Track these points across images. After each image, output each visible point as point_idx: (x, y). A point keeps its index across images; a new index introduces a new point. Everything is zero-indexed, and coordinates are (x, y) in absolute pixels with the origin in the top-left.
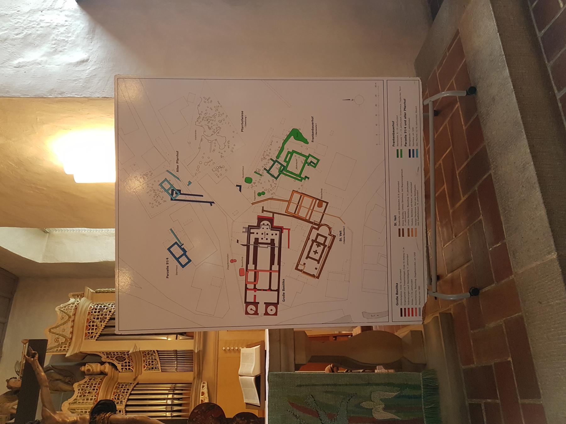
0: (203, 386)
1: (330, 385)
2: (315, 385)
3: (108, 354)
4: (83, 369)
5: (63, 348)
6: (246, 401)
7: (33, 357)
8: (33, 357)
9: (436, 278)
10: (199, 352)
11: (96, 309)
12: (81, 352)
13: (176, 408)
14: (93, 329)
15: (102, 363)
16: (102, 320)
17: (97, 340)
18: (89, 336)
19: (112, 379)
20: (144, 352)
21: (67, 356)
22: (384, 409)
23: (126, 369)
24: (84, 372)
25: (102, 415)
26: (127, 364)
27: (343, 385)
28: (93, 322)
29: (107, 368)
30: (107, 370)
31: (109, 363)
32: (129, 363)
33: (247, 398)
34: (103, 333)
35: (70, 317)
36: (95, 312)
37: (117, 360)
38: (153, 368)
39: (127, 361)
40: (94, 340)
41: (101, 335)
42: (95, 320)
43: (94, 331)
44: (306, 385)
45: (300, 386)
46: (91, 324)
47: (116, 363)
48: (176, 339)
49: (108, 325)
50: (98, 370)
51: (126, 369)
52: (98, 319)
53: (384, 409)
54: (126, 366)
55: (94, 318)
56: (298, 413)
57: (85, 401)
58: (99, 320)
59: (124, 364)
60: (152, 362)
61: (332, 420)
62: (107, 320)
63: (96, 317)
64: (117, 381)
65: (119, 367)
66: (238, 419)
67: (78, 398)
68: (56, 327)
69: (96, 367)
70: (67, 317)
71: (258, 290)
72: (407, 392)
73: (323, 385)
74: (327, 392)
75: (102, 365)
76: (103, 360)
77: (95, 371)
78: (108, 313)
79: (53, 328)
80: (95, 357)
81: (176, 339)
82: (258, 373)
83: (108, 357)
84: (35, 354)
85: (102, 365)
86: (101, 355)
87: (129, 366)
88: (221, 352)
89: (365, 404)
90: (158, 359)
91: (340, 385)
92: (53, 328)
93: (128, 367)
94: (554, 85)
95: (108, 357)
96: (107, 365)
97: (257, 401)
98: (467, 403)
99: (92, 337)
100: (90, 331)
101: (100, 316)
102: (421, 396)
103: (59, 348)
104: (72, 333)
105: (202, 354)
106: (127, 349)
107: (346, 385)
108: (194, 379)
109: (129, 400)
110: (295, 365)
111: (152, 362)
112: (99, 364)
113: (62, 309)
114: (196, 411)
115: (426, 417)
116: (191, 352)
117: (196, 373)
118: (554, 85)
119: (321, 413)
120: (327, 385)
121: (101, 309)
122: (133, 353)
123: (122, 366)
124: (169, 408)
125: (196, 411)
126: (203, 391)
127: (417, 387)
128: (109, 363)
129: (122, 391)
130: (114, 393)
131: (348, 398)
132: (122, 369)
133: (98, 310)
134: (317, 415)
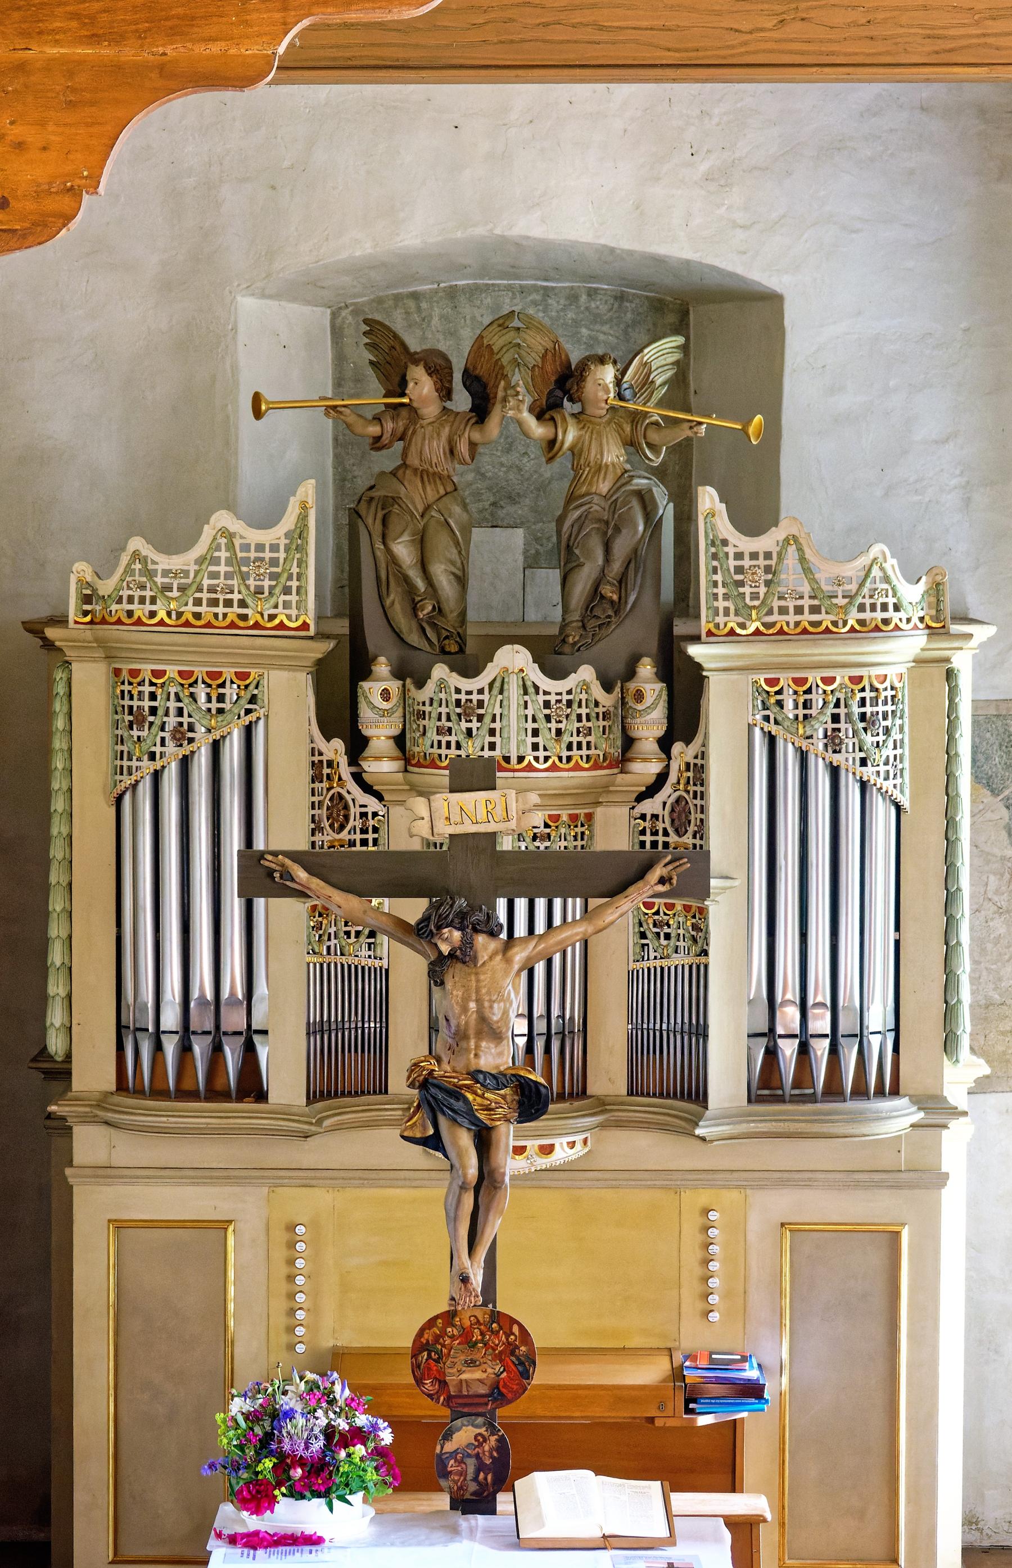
0: (572, 1145)
3: (698, 772)
5: (721, 604)
15: (665, 744)
21: (694, 650)
23: (643, 832)
29: (647, 769)
30: (636, 767)
37: (678, 800)
38: (643, 935)
47: (666, 792)
51: (643, 832)
54: (655, 833)
55: (837, 705)
57: (530, 725)
59: (660, 826)
60: (668, 936)
63: (842, 711)
65: (649, 806)
66: (493, 1438)
67: (541, 698)
68: (802, 559)
69: (651, 722)
76: (677, 747)
79: (800, 550)
80: (684, 720)
86: (698, 740)
88: (695, 1199)
92: (800, 550)
93: (648, 838)
94: (63, 51)
96: (654, 768)
103: (721, 591)
113: (876, 572)
118: (63, 51)
123: (655, 817)
125: (516, 1329)
126: (557, 1147)
130: (556, 818)
132: (643, 817)
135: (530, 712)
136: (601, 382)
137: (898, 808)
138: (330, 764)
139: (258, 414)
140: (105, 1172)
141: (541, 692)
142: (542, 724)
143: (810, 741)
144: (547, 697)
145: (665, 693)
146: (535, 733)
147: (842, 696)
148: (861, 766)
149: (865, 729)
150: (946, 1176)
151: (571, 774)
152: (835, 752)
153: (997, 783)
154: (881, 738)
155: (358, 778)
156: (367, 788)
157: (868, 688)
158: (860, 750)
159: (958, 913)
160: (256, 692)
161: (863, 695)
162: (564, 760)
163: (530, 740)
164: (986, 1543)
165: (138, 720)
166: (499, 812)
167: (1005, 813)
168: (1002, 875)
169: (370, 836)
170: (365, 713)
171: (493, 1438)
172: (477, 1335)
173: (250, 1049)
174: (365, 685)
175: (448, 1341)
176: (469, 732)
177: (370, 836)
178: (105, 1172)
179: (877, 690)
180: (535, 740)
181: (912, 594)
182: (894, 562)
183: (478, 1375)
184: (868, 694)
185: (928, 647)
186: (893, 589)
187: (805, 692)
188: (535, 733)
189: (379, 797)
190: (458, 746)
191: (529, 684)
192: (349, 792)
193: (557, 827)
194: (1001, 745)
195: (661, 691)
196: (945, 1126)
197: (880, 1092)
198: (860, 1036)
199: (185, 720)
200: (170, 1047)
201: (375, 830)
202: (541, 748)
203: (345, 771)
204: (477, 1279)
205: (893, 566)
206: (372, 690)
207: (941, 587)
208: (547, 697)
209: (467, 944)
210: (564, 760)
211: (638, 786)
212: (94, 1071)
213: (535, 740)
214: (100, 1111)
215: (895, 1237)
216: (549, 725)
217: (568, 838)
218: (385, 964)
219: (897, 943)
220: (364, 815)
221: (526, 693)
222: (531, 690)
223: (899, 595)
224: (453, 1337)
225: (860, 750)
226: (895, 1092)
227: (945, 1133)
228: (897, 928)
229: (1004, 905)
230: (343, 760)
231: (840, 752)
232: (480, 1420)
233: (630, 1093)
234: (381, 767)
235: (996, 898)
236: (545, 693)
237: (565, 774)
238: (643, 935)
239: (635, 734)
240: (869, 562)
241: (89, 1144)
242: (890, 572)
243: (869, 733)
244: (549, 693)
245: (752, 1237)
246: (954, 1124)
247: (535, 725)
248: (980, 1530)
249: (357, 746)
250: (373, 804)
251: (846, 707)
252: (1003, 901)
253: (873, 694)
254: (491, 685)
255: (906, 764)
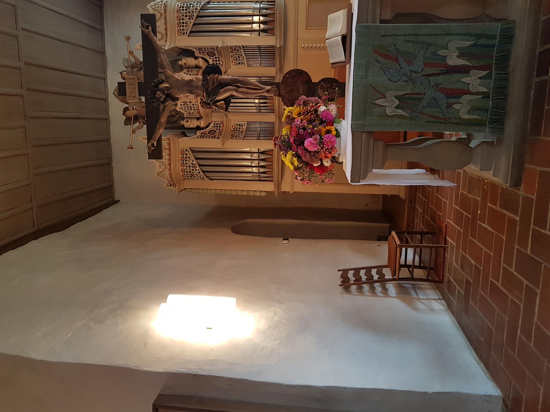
1: (412, 35)
2: (398, 35)
3: (200, 49)
4: (180, 62)
6: (332, 61)
7: (148, 29)
8: (148, 29)
10: (280, 47)
11: (183, 7)
12: (176, 47)
14: (183, 26)
15: (196, 58)
16: (191, 18)
17: (188, 36)
18: (181, 32)
20: (231, 47)
22: (458, 57)
24: (182, 66)
25: (212, 75)
26: (217, 59)
27: (423, 35)
28: (183, 19)
31: (202, 58)
32: (219, 58)
33: (332, 59)
34: (193, 30)
35: (161, 14)
36: (183, 10)
38: (240, 63)
39: (216, 56)
40: (185, 36)
41: (191, 32)
42: (184, 17)
43: (185, 28)
44: (390, 35)
45: (384, 36)
46: (181, 21)
47: (207, 58)
48: (259, 35)
49: (196, 22)
50: (194, 64)
52: (186, 16)
53: (458, 57)
56: (380, 59)
58: (188, 17)
60: (239, 57)
61: (409, 65)
62: (194, 18)
63: (185, 15)
66: (322, 83)
69: (191, 61)
70: (159, 15)
72: (483, 41)
73: (405, 35)
74: (408, 41)
75: (196, 59)
77: (191, 64)
78: (195, 10)
80: (188, 52)
81: (259, 35)
82: (344, 32)
83: (200, 52)
84: (148, 26)
85: (196, 59)
86: (194, 50)
87: (219, 61)
88: (300, 49)
89: (441, 52)
90: (244, 55)
91: (420, 35)
95: (200, 52)
96: (200, 60)
97: (342, 58)
98: (537, 52)
99: (184, 34)
100: (182, 28)
101: (188, 14)
102: (496, 36)
104: (166, 29)
105: (283, 48)
106: (216, 45)
107: (426, 35)
108: (277, 73)
110: (381, 20)
111: (239, 57)
112: (194, 59)
113: (153, 7)
114: (287, 76)
115: (495, 64)
116: (273, 47)
117: (278, 68)
119: (401, 59)
120: (409, 35)
121: (188, 8)
122: (222, 47)
125: (287, 76)
127: (494, 37)
128: (202, 58)
131: (426, 47)
133: (185, 8)
134: (396, 60)
138: (202, 134)
139: (132, 148)
155: (206, 127)
156: (208, 126)
165: (192, 175)
166: (132, 81)
170: (191, 126)
171: (322, 83)
172: (289, 88)
173: (262, 153)
174: (185, 126)
175: (290, 98)
176: (190, 102)
183: (301, 88)
184: (181, 9)
189: (210, 123)
190: (193, 105)
197: (274, 5)
198: (261, 9)
199: (191, 165)
200: (262, 170)
204: (268, 87)
206: (186, 125)
209: (162, 90)
212: (269, 187)
214: (278, 186)
224: (289, 96)
230: (202, 131)
232: (316, 88)
234: (202, 124)
238: (240, 63)
239: (194, 66)
249: (198, 128)
250: (212, 125)
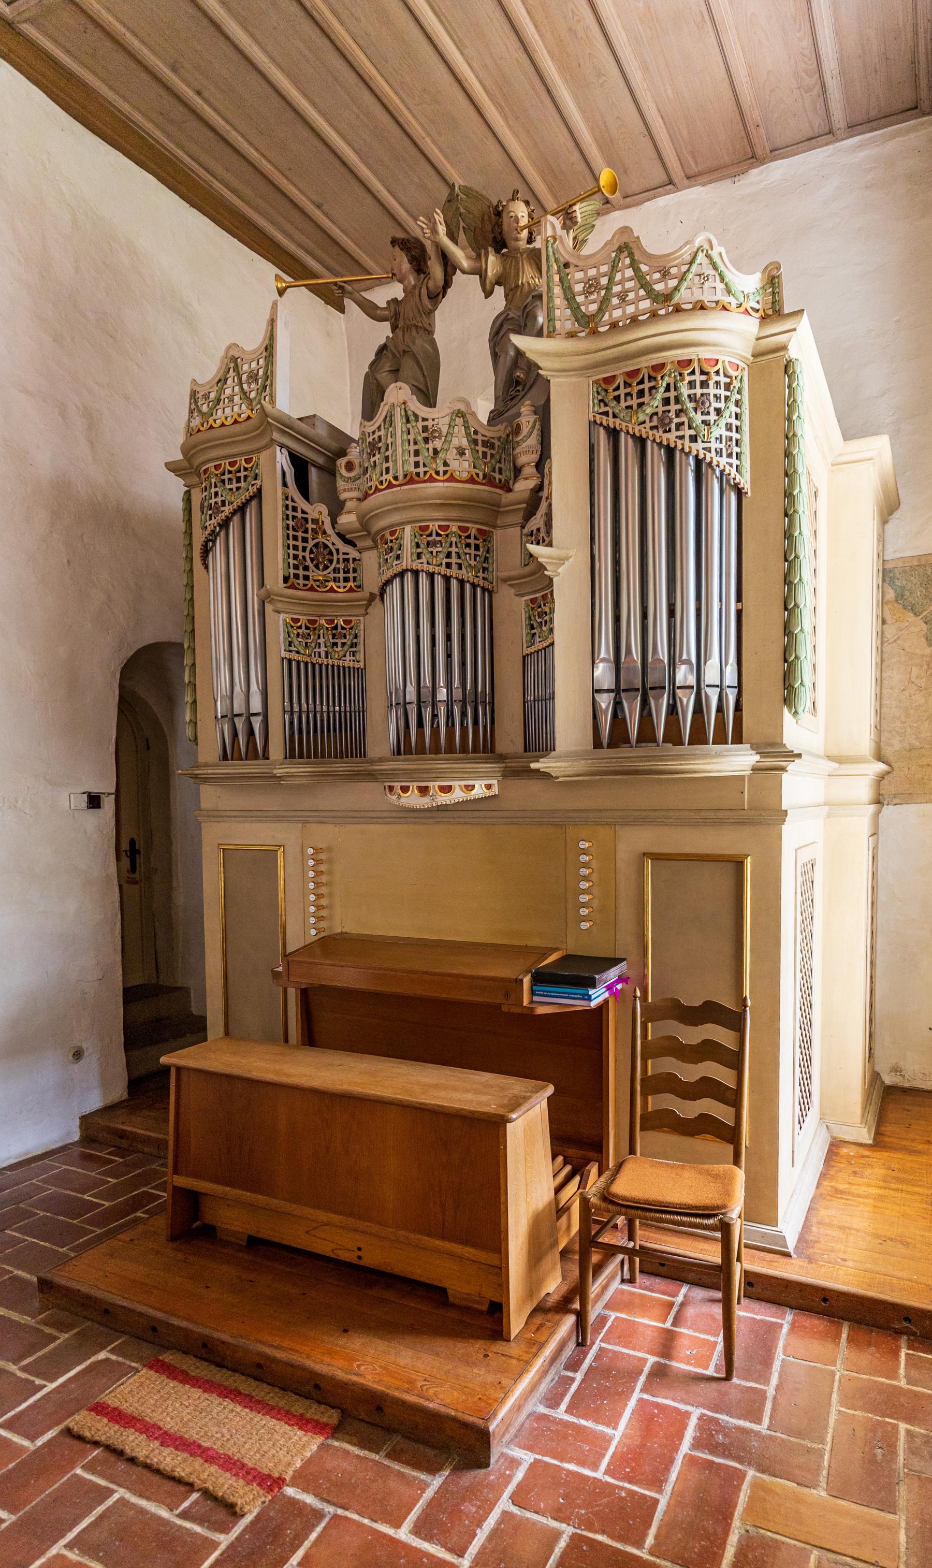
9: (869, 1344)
13: (427, 714)
19: (494, 510)
36: (692, 384)
38: (532, 628)
55: (668, 389)
57: (412, 448)
64: (495, 527)
67: (420, 424)
71: (877, 814)
109: (431, 576)
113: (701, 257)
124: (426, 694)
129: (454, 550)
135: (411, 437)
136: (512, 214)
137: (740, 493)
138: (315, 521)
140: (216, 815)
141: (420, 420)
142: (421, 445)
143: (643, 425)
144: (425, 423)
145: (538, 426)
146: (417, 453)
147: (672, 381)
148: (691, 442)
149: (695, 410)
150: (786, 812)
151: (447, 484)
152: (665, 432)
153: (918, 608)
154: (713, 417)
157: (697, 371)
158: (690, 428)
159: (795, 578)
160: (399, 552)
161: (692, 378)
162: (441, 473)
163: (412, 459)
164: (907, 1085)
167: (924, 627)
168: (922, 666)
169: (351, 575)
177: (351, 575)
178: (216, 815)
179: (707, 374)
180: (417, 459)
181: (748, 283)
182: (722, 250)
184: (698, 378)
185: (762, 335)
186: (720, 275)
187: (638, 384)
188: (417, 453)
191: (410, 413)
192: (333, 544)
193: (447, 535)
194: (921, 584)
195: (535, 422)
196: (783, 769)
201: (355, 571)
202: (421, 465)
203: (328, 526)
205: (720, 254)
207: (776, 280)
208: (425, 423)
210: (441, 473)
211: (520, 503)
213: (417, 459)
215: (739, 865)
216: (427, 446)
217: (459, 545)
218: (362, 665)
219: (739, 613)
220: (346, 560)
221: (408, 421)
222: (412, 418)
223: (727, 280)
225: (690, 428)
226: (738, 739)
227: (785, 776)
228: (739, 599)
229: (923, 685)
231: (670, 430)
233: (525, 751)
235: (917, 681)
236: (424, 420)
237: (441, 484)
240: (695, 250)
241: (210, 797)
242: (716, 259)
243: (699, 413)
244: (427, 420)
245: (620, 864)
246: (791, 767)
247: (416, 447)
248: (904, 1076)
251: (675, 390)
252: (923, 683)
253: (704, 378)
254: (385, 420)
255: (746, 448)
